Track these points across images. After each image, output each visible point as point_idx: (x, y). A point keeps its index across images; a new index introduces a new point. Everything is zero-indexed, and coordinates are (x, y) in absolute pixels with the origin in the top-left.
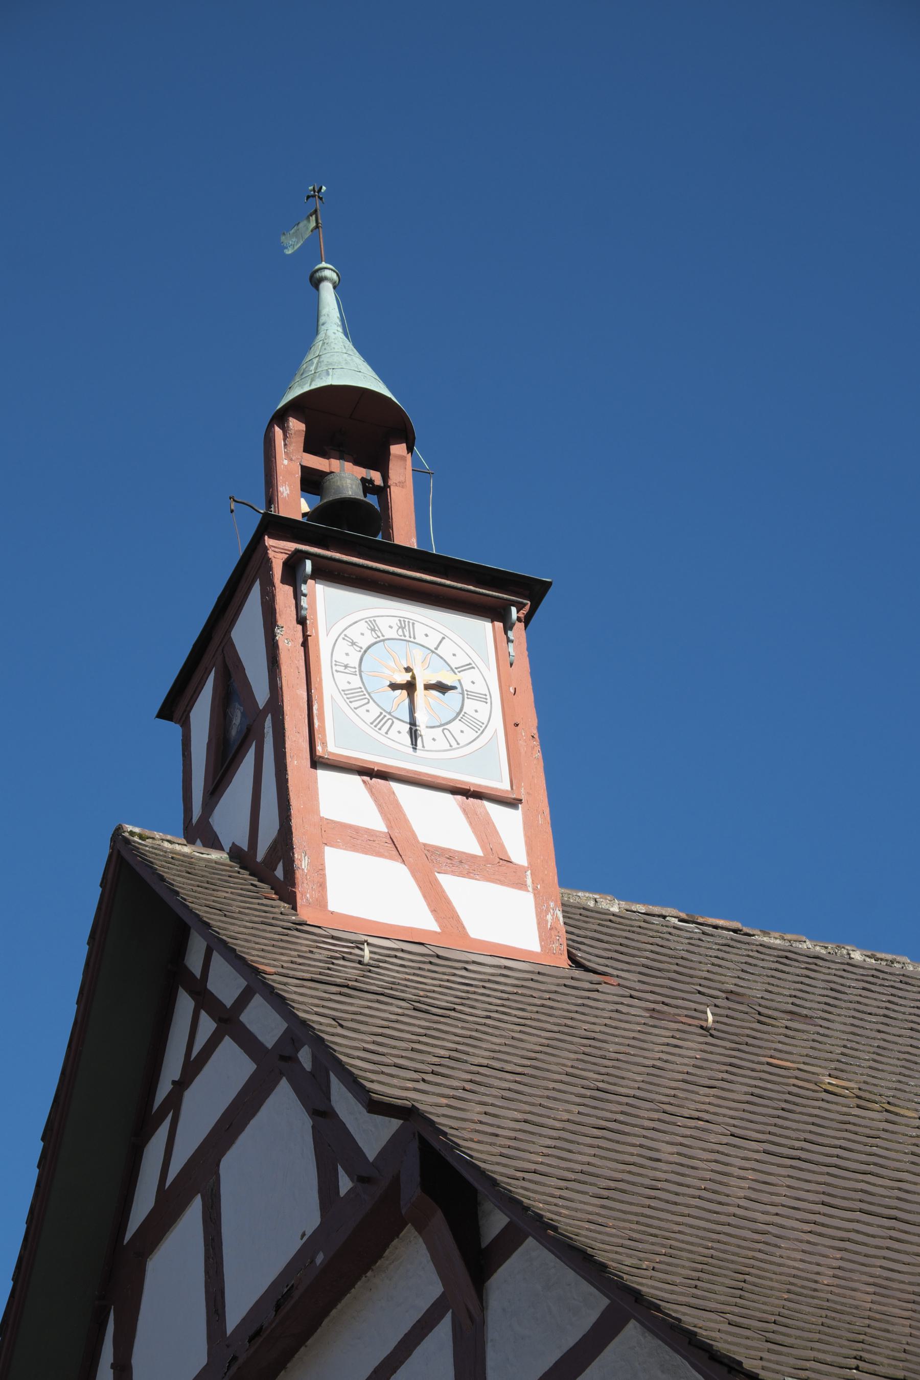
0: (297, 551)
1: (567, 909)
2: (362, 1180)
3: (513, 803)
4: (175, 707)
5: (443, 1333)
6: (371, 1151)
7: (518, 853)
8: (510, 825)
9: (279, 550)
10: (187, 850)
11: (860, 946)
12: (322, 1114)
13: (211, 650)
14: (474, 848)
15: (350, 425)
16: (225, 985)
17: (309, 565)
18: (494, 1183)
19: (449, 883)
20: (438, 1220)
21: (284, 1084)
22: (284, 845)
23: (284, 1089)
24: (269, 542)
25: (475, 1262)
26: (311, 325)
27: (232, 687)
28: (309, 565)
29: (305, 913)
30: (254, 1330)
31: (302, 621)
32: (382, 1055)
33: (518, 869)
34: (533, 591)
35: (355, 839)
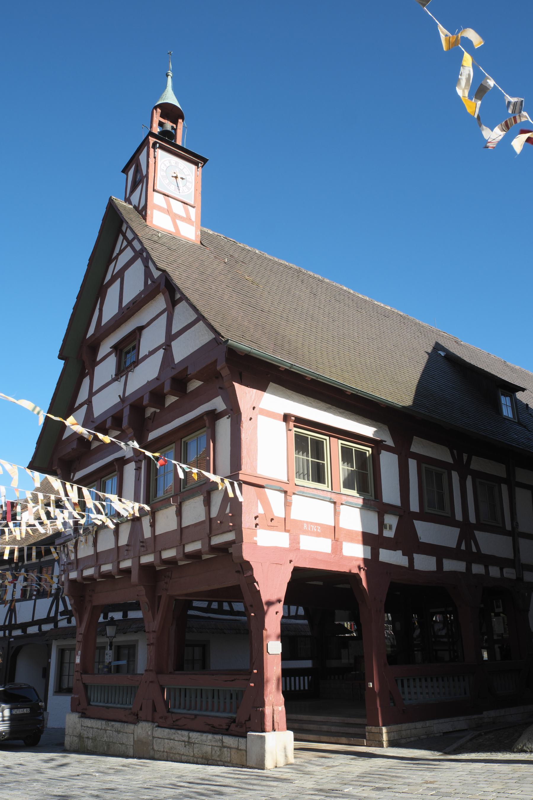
0: (156, 141)
1: (202, 232)
2: (153, 282)
3: (194, 207)
4: (125, 171)
5: (165, 315)
6: (156, 277)
7: (193, 218)
8: (192, 212)
9: (152, 140)
10: (125, 204)
11: (258, 249)
12: (147, 267)
13: (134, 160)
14: (185, 216)
15: (171, 113)
16: (130, 236)
17: (158, 145)
18: (179, 289)
19: (178, 222)
20: (167, 293)
21: (140, 259)
22: (145, 207)
23: (139, 261)
24: (150, 138)
25: (173, 302)
26: (165, 87)
27: (138, 169)
28: (158, 145)
29: (148, 223)
30: (128, 307)
31: (155, 158)
32: (162, 259)
33: (193, 222)
34: (205, 160)
35: (160, 209)
